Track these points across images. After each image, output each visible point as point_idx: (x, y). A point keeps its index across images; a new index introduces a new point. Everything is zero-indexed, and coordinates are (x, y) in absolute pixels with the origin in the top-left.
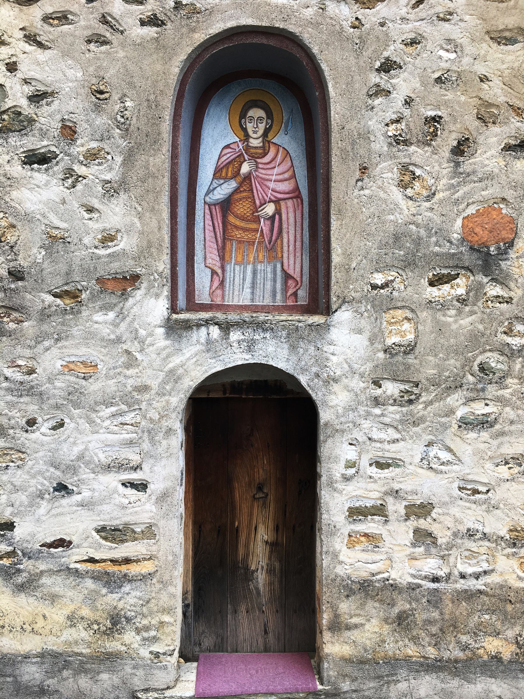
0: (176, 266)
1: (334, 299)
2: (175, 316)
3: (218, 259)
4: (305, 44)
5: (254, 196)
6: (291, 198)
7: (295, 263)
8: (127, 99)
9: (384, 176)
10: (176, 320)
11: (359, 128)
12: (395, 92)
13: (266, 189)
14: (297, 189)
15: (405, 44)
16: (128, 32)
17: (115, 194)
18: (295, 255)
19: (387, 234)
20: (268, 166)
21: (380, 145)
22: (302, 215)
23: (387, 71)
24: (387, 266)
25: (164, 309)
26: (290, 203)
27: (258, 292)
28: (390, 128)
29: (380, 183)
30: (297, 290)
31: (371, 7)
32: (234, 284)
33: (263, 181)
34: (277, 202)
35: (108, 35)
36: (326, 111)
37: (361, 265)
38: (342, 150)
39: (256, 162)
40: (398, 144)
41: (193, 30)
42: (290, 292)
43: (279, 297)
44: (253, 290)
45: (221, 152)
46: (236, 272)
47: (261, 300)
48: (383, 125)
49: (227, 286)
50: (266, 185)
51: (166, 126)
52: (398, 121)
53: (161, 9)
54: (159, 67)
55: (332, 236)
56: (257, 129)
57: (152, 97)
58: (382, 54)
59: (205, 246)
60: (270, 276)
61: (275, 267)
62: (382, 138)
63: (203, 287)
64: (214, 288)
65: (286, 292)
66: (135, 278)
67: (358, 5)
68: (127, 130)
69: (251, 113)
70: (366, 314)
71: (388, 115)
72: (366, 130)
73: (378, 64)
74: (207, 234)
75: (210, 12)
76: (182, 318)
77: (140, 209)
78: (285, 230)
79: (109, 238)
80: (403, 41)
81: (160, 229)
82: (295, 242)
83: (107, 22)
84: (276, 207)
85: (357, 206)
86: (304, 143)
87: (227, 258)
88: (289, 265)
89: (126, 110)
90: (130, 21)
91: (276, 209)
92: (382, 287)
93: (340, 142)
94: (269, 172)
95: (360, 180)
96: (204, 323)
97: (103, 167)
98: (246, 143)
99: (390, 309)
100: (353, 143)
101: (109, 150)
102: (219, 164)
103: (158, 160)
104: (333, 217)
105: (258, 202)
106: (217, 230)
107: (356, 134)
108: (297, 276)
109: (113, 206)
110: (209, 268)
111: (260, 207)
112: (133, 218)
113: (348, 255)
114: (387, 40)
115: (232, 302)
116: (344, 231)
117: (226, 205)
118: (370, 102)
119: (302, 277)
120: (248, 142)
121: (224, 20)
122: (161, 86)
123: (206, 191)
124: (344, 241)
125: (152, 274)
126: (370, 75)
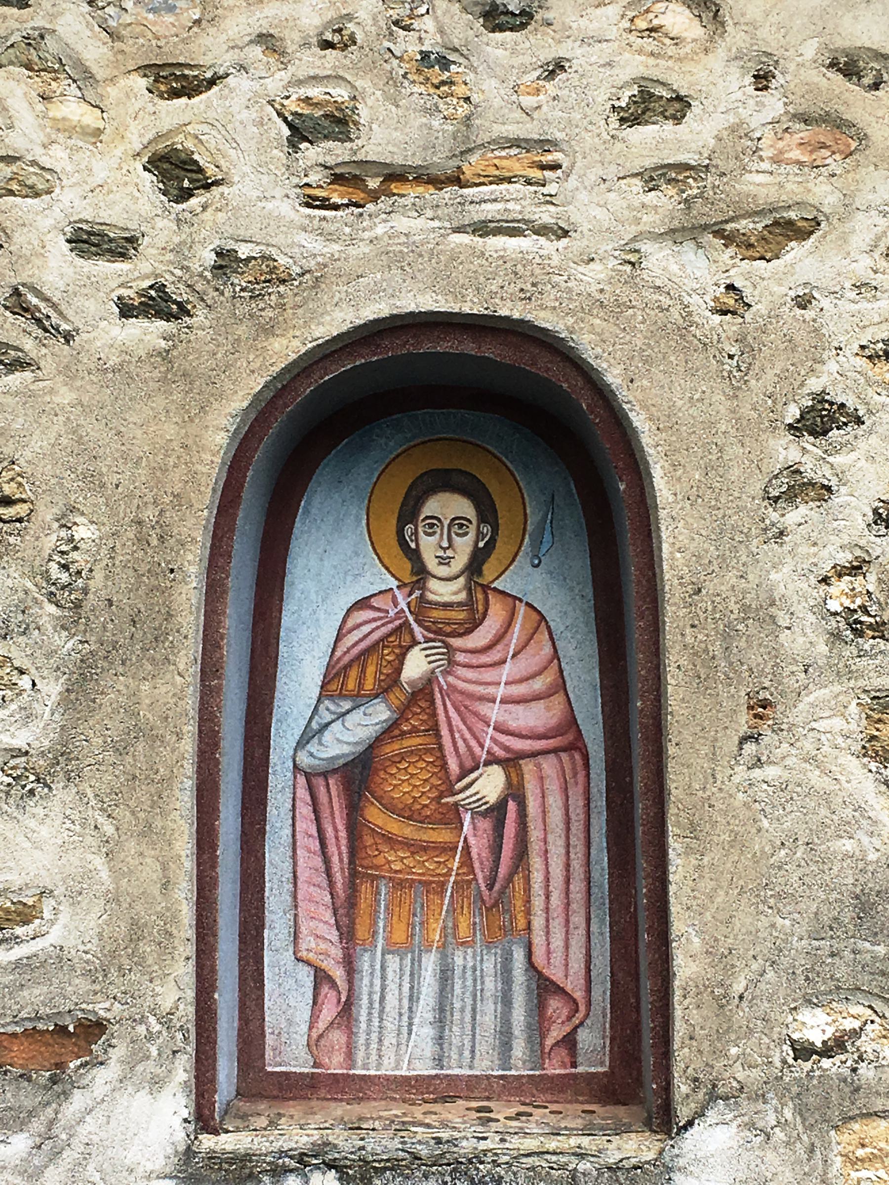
0: (213, 988)
1: (681, 1088)
2: (208, 1142)
3: (334, 935)
4: (584, 360)
5: (441, 748)
6: (555, 751)
7: (567, 947)
8: (79, 519)
9: (820, 725)
10: (211, 1156)
11: (744, 592)
12: (844, 490)
13: (480, 725)
14: (571, 723)
15: (869, 357)
16: (85, 336)
17: (40, 789)
18: (567, 921)
19: (835, 895)
20: (485, 659)
21: (805, 638)
22: (588, 800)
23: (819, 432)
24: (838, 988)
25: (177, 1122)
26: (549, 765)
27: (456, 1035)
28: (834, 590)
29: (808, 745)
30: (576, 1027)
31: (768, 255)
32: (382, 1011)
33: (468, 705)
34: (511, 762)
35: (28, 344)
36: (649, 535)
37: (762, 986)
38: (695, 654)
39: (447, 646)
40: (859, 633)
41: (268, 330)
42: (556, 1033)
43: (519, 1049)
44: (442, 1029)
45: (344, 621)
46: (390, 975)
47: (467, 1061)
48: (813, 581)
49: (363, 1018)
50: (476, 714)
51: (189, 593)
52: (856, 569)
53: (178, 272)
54: (170, 431)
55: (672, 900)
56: (449, 553)
57: (150, 514)
58: (802, 385)
59: (295, 897)
60: (490, 984)
61: (507, 960)
62: (812, 618)
63: (290, 1022)
64: (322, 1025)
65: (543, 1037)
66: (93, 1029)
67: (732, 250)
68: (77, 605)
69: (433, 506)
70: (779, 1135)
71: (825, 553)
72: (763, 596)
73: (792, 413)
74: (301, 862)
75: (316, 279)
76: (229, 1148)
77: (109, 829)
78: (535, 847)
79: (19, 914)
80: (863, 347)
81: (166, 885)
82: (567, 881)
83: (26, 310)
84: (508, 777)
85: (743, 813)
86: (589, 592)
87: (361, 932)
88: (549, 952)
89: (76, 548)
90: (91, 306)
91: (509, 783)
92: (827, 1051)
93: (688, 630)
94: (488, 675)
95: (752, 738)
96: (293, 1164)
97: (7, 712)
98: (417, 593)
99: (852, 1118)
100: (728, 634)
101: (25, 664)
102: (338, 654)
103: (163, 689)
104: (675, 847)
105: (453, 766)
106: (332, 849)
107: (735, 608)
108: (574, 985)
109: (32, 824)
110: (308, 963)
111: (460, 779)
112: (91, 857)
113: (723, 956)
114: (818, 347)
115: (379, 1066)
116: (706, 885)
117: (358, 775)
118: (774, 516)
119: (588, 990)
120: (424, 588)
121: (352, 301)
122: (175, 480)
123: (298, 733)
124: (708, 916)
125: (143, 1020)
126: (771, 442)
